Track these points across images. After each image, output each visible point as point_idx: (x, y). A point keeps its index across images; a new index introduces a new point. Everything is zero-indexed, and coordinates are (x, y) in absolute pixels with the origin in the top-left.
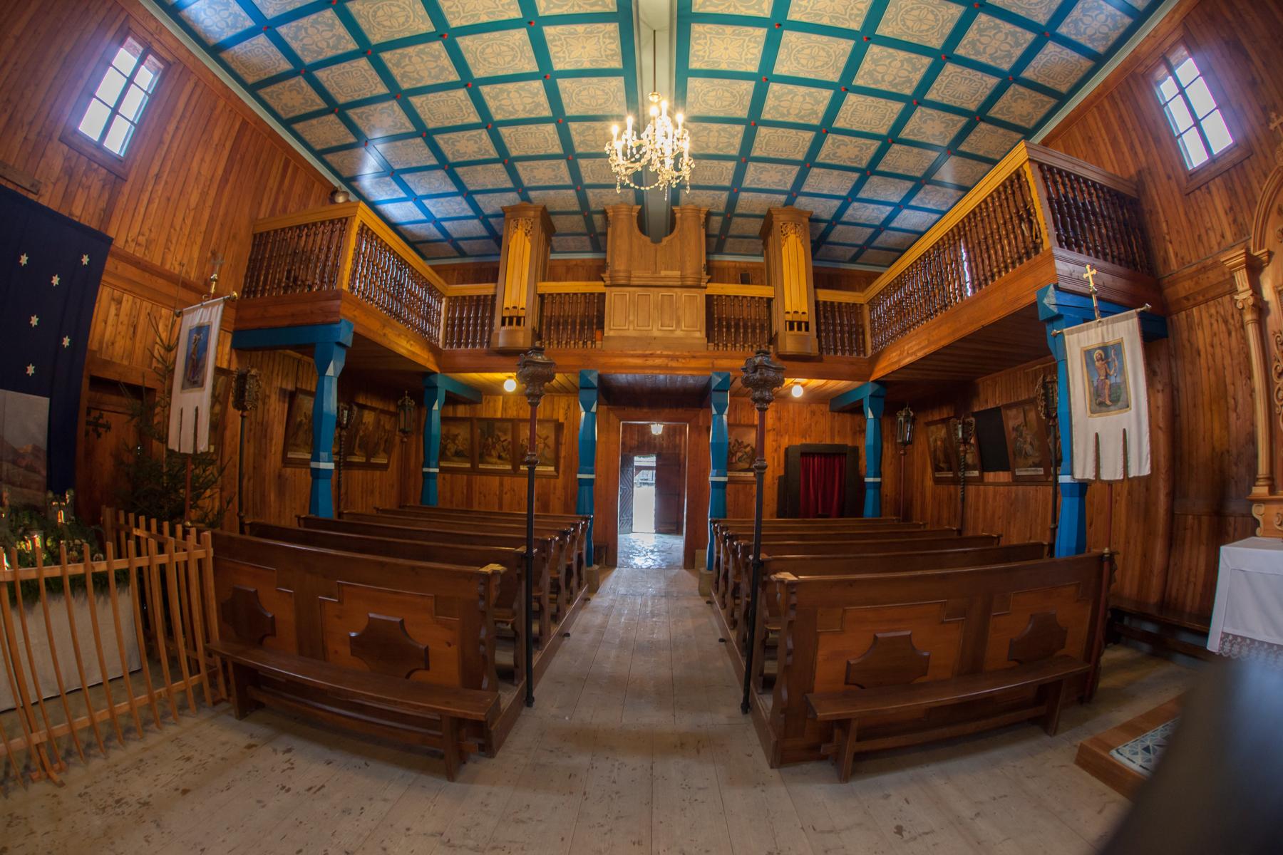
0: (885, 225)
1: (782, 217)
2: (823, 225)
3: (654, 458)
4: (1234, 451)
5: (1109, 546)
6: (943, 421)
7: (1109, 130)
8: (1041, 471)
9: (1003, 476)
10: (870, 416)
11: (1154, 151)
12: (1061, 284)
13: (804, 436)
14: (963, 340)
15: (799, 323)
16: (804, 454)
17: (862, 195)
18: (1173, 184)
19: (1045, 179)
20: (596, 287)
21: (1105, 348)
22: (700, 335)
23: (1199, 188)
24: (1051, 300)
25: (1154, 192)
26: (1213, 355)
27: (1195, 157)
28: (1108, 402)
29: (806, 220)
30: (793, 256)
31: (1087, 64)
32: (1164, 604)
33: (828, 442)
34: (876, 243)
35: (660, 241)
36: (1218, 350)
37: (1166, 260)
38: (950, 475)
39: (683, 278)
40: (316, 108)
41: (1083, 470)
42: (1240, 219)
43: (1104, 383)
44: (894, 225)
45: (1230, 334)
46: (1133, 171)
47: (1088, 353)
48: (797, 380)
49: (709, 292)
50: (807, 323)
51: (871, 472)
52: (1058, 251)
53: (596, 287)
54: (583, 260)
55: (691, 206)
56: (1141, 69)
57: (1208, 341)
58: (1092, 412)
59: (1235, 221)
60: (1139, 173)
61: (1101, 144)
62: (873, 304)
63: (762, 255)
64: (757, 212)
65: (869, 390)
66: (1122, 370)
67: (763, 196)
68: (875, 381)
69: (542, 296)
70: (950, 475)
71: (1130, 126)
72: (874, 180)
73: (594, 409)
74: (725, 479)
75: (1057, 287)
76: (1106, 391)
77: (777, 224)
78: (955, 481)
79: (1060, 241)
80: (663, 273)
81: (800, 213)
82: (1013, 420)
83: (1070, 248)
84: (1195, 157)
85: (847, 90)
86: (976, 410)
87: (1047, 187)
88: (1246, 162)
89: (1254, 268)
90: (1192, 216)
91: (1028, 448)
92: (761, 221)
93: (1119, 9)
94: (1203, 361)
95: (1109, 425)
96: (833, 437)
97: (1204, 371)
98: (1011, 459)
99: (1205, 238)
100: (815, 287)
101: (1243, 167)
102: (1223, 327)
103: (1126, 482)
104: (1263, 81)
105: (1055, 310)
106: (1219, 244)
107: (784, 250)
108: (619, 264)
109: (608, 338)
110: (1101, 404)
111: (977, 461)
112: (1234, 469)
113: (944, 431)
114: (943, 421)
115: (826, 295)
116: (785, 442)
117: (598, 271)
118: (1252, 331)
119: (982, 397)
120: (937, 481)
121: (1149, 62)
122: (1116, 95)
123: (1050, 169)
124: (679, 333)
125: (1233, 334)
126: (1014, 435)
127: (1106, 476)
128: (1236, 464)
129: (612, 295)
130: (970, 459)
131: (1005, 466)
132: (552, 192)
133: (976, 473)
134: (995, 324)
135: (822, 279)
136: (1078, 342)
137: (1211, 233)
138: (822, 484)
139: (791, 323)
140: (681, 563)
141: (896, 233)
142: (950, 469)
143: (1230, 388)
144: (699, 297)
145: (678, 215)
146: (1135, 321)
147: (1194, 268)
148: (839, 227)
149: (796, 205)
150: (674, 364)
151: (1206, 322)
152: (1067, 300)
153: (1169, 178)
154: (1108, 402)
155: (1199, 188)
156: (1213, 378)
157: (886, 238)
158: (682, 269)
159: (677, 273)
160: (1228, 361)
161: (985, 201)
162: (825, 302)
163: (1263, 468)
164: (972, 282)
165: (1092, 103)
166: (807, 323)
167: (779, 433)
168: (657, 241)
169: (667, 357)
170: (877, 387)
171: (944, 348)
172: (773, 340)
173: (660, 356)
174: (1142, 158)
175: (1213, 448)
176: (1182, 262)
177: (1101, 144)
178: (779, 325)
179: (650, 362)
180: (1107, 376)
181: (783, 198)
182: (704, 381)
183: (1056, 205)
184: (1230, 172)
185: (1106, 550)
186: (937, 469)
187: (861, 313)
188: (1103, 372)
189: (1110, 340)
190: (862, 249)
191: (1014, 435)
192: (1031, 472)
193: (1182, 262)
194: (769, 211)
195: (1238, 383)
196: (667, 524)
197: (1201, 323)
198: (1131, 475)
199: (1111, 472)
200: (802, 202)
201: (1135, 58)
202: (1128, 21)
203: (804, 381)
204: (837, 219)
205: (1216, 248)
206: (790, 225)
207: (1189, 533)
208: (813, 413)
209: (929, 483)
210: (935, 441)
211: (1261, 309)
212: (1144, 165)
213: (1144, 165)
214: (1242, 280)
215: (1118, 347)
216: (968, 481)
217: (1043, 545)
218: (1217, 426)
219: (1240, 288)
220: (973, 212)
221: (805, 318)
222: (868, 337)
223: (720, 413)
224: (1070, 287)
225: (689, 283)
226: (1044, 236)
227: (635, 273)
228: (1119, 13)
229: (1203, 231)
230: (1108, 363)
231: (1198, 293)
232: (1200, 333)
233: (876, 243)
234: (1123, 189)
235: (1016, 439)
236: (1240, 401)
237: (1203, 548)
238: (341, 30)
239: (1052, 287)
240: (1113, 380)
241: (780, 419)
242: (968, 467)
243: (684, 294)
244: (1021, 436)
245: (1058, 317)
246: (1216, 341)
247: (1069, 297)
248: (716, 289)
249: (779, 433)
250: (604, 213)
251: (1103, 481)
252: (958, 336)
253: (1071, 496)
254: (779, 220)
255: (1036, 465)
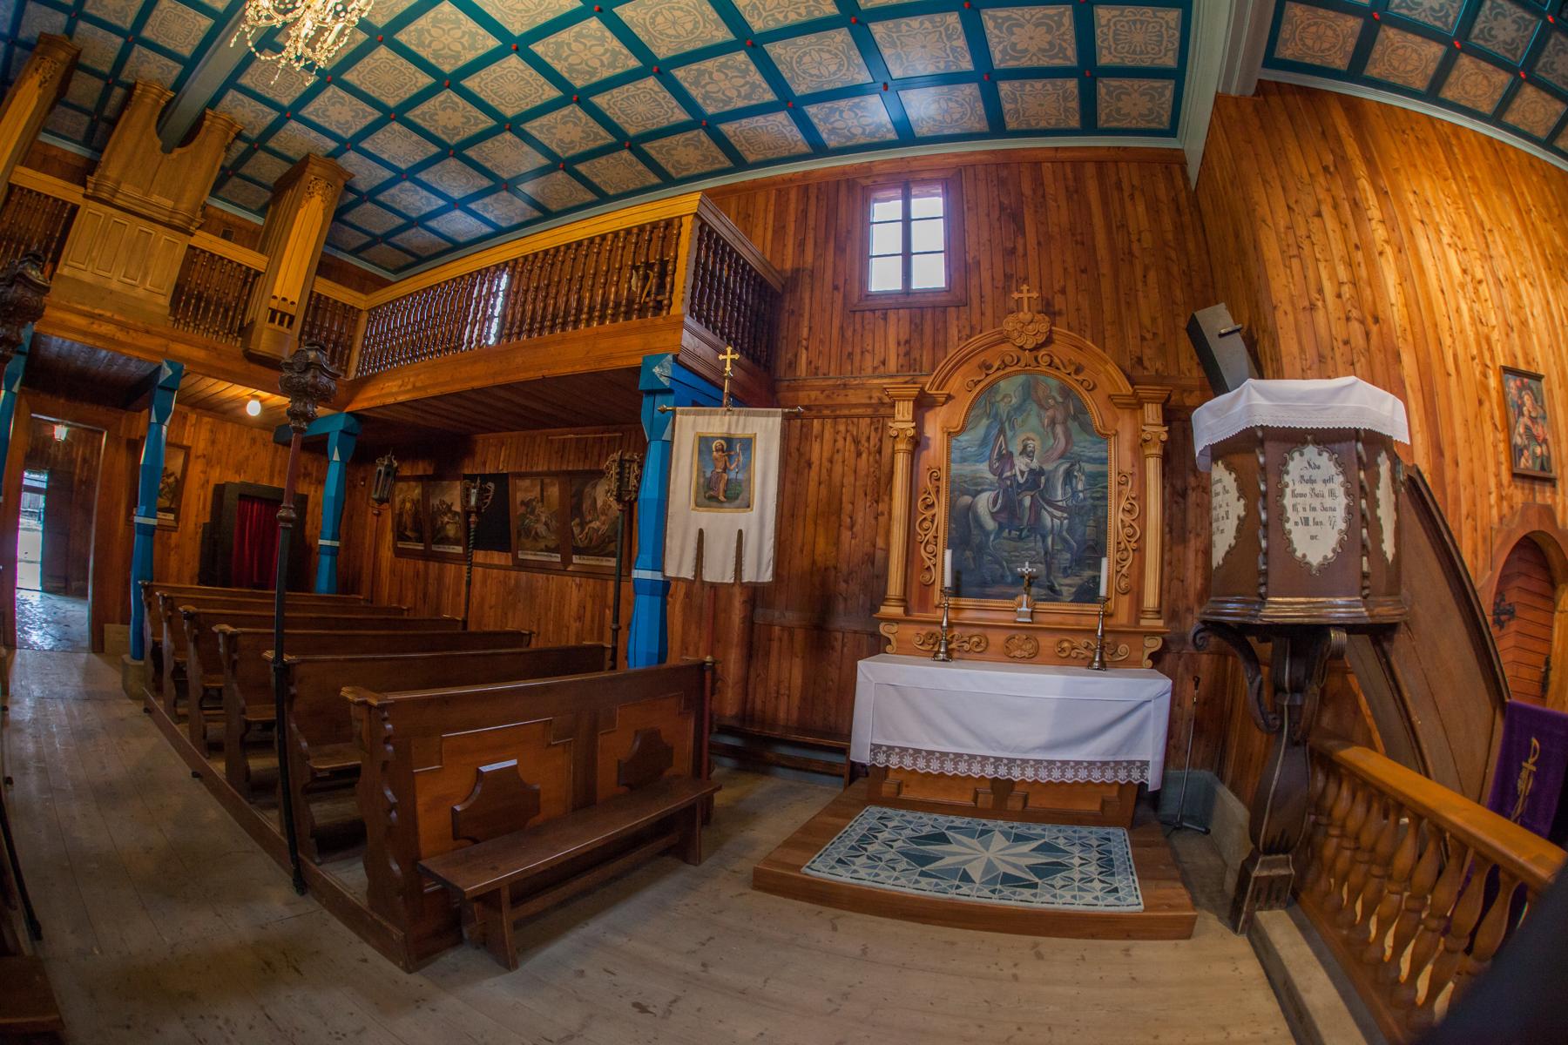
0: (421, 221)
1: (317, 170)
2: (352, 197)
3: (45, 477)
4: (844, 568)
5: (712, 654)
6: (418, 478)
7: (780, 217)
8: (557, 558)
9: (498, 558)
10: (336, 457)
11: (830, 259)
12: (682, 357)
13: (238, 472)
14: (507, 387)
15: (284, 315)
16: (242, 497)
17: (423, 176)
18: (839, 297)
19: (700, 240)
20: (70, 192)
21: (729, 440)
22: (165, 301)
23: (873, 311)
24: (662, 372)
25: (807, 296)
26: (830, 471)
27: (883, 277)
28: (722, 498)
29: (341, 183)
30: (307, 222)
31: (803, 146)
32: (746, 715)
33: (265, 483)
34: (396, 239)
35: (171, 152)
36: (838, 468)
37: (792, 365)
38: (420, 547)
39: (174, 211)
40: (600, 143)
41: (679, 565)
42: (915, 354)
43: (719, 476)
44: (433, 224)
45: (859, 454)
46: (788, 265)
47: (704, 442)
48: (259, 393)
49: (194, 241)
50: (292, 318)
51: (329, 532)
52: (688, 320)
53: (70, 192)
54: (66, 153)
55: (225, 116)
56: (869, 182)
57: (826, 455)
58: (697, 505)
59: (907, 354)
60: (797, 271)
61: (761, 226)
62: (373, 311)
63: (262, 211)
64: (290, 154)
65: (340, 423)
66: (747, 467)
67: (314, 134)
68: (350, 413)
69: (11, 187)
70: (420, 547)
71: (811, 223)
72: (452, 163)
73: (16, 389)
74: (153, 522)
75: (676, 358)
76: (722, 486)
77: (309, 176)
78: (428, 556)
79: (692, 310)
80: (155, 198)
81: (340, 172)
82: (523, 492)
83: (699, 320)
84: (883, 277)
85: (517, 50)
86: (467, 471)
87: (699, 249)
88: (952, 311)
89: (923, 404)
90: (849, 333)
91: (541, 529)
92: (287, 167)
93: (894, 123)
94: (814, 474)
95: (721, 523)
96: (272, 477)
97: (813, 485)
98: (514, 536)
99: (857, 357)
100: (318, 273)
101: (944, 312)
102: (850, 446)
103: (737, 590)
104: (1025, 255)
105: (666, 382)
106: (875, 369)
107: (301, 213)
108: (112, 167)
109: (61, 277)
110: (711, 498)
111: (460, 534)
112: (843, 586)
113: (418, 491)
114: (418, 478)
115: (326, 287)
116: (216, 476)
117: (81, 173)
118: (901, 462)
119: (478, 459)
120: (399, 553)
121: (880, 180)
122: (813, 192)
123: (712, 231)
124: (140, 292)
125: (864, 456)
126: (522, 510)
127: (708, 577)
128: (846, 582)
129: (91, 214)
130: (451, 531)
131: (503, 544)
132: (101, 32)
133: (459, 549)
134: (557, 379)
135: (325, 267)
136: (692, 427)
137: (868, 356)
138: (251, 540)
139: (274, 312)
140: (86, 644)
141: (427, 234)
142: (420, 540)
143: (847, 507)
144: (181, 243)
145: (207, 123)
146: (779, 420)
147: (830, 382)
148: (369, 205)
149: (340, 161)
150: (120, 336)
151: (827, 435)
152: (684, 375)
153: (836, 288)
154: (722, 498)
155: (873, 311)
156: (824, 490)
157: (416, 238)
158: (177, 200)
159: (169, 204)
160: (849, 479)
161: (603, 237)
162: (319, 295)
163: (895, 586)
164: (503, 317)
165: (774, 184)
166: (292, 318)
167: (209, 462)
168: (167, 150)
169: (118, 323)
170: (352, 420)
171: (473, 390)
172: (245, 331)
173: (110, 321)
174: (809, 257)
175: (814, 562)
176: (814, 371)
177: (761, 226)
178: (258, 312)
179: (95, 328)
180: (725, 470)
181: (332, 145)
182: (146, 370)
183: (702, 272)
184: (913, 307)
185: (708, 658)
186: (400, 535)
187: (356, 321)
188: (721, 465)
189: (738, 432)
190: (376, 240)
191: (522, 510)
192: (542, 557)
193: (814, 371)
194: (308, 156)
195: (860, 503)
196: (59, 580)
197: (821, 436)
198: (745, 580)
199: (718, 571)
200: (351, 159)
201: (867, 169)
202: (892, 136)
203: (265, 395)
204: (371, 196)
205: (870, 370)
206: (322, 184)
207: (775, 645)
208: (254, 441)
209: (386, 553)
210: (404, 502)
211: (918, 443)
212: (809, 266)
213: (809, 266)
214: (904, 411)
215: (748, 443)
216: (443, 558)
217: (604, 648)
218: (821, 542)
219: (898, 417)
220: (579, 244)
221: (292, 310)
222: (355, 356)
223: (161, 422)
224: (689, 362)
225: (177, 222)
226: (677, 299)
227: (126, 188)
228: (890, 126)
229: (858, 351)
230: (730, 456)
231: (827, 407)
232: (816, 446)
233: (396, 239)
234: (769, 279)
235: (524, 515)
236: (860, 521)
237: (797, 661)
238: (756, 77)
239: (670, 357)
240: (732, 475)
241: (213, 442)
242: (446, 540)
243: (163, 236)
244: (532, 512)
245: (669, 391)
246: (838, 457)
247: (685, 372)
248: (206, 241)
249: (209, 462)
250: (130, 88)
251: (703, 583)
252: (501, 380)
253: (652, 594)
254: (314, 170)
255: (548, 549)
